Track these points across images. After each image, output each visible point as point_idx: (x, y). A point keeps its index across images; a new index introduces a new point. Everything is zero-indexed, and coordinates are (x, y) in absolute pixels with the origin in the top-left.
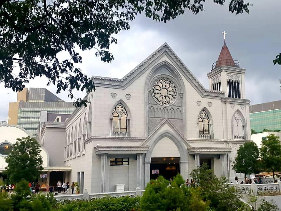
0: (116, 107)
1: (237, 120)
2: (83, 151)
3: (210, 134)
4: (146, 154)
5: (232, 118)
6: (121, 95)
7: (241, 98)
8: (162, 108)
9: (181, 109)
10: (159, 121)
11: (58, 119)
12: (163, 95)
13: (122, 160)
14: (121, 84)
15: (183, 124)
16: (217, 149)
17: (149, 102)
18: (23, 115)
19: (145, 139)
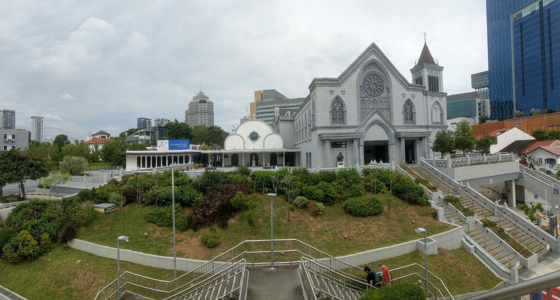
2: (309, 137)
3: (413, 121)
4: (360, 138)
5: (432, 108)
6: (337, 91)
7: (440, 92)
8: (372, 100)
9: (388, 101)
11: (288, 113)
13: (341, 143)
14: (337, 83)
15: (390, 113)
16: (419, 132)
18: (259, 111)
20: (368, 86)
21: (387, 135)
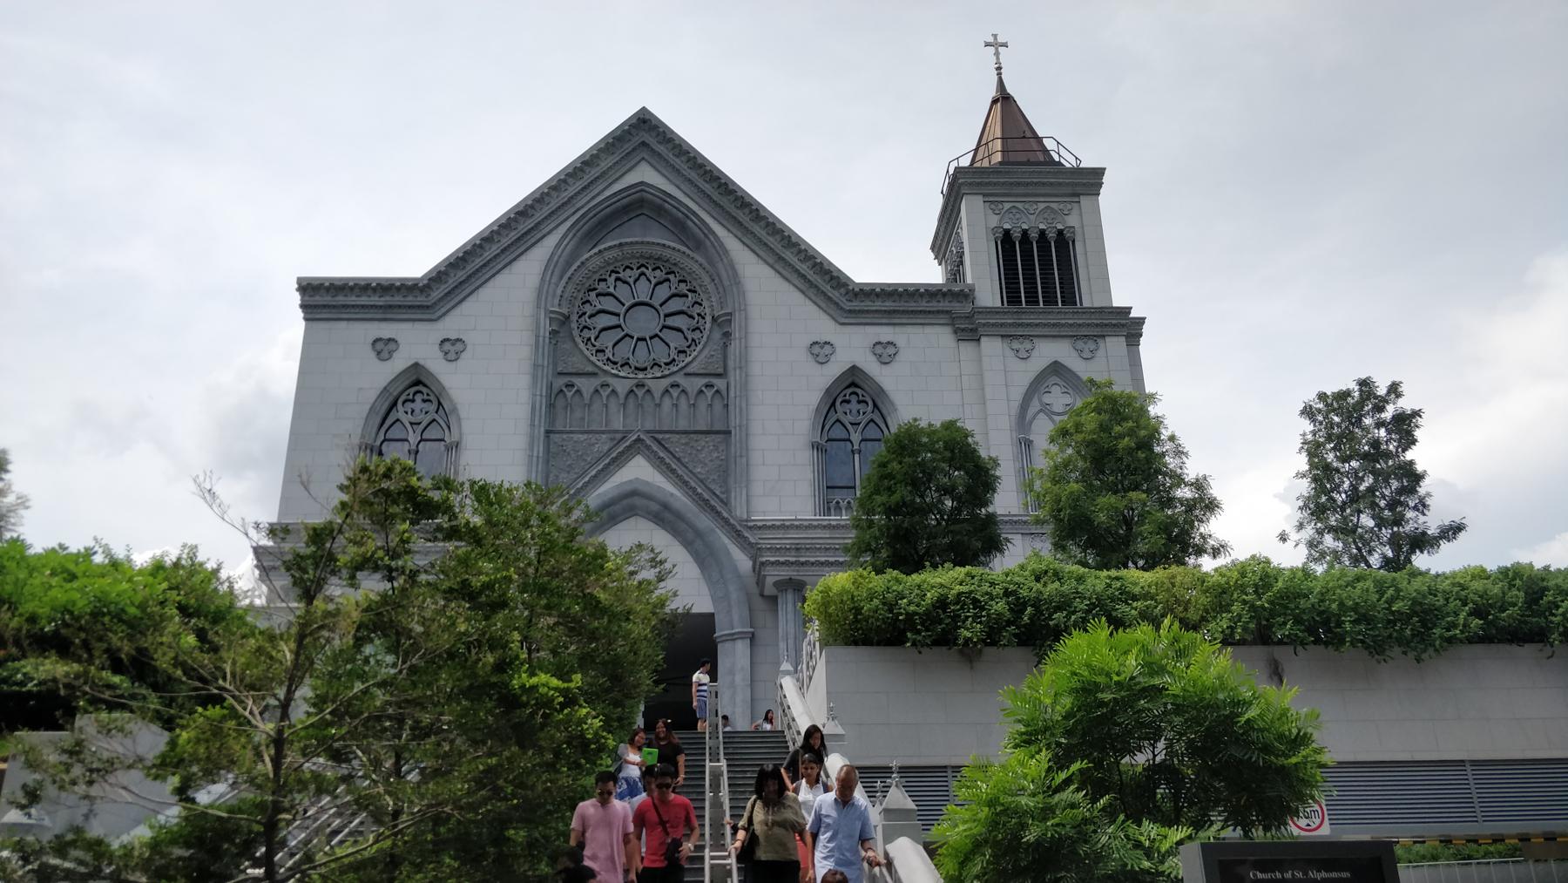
1: (1056, 418)
7: (1086, 304)
10: (606, 448)
12: (652, 334)
14: (421, 300)
17: (555, 365)
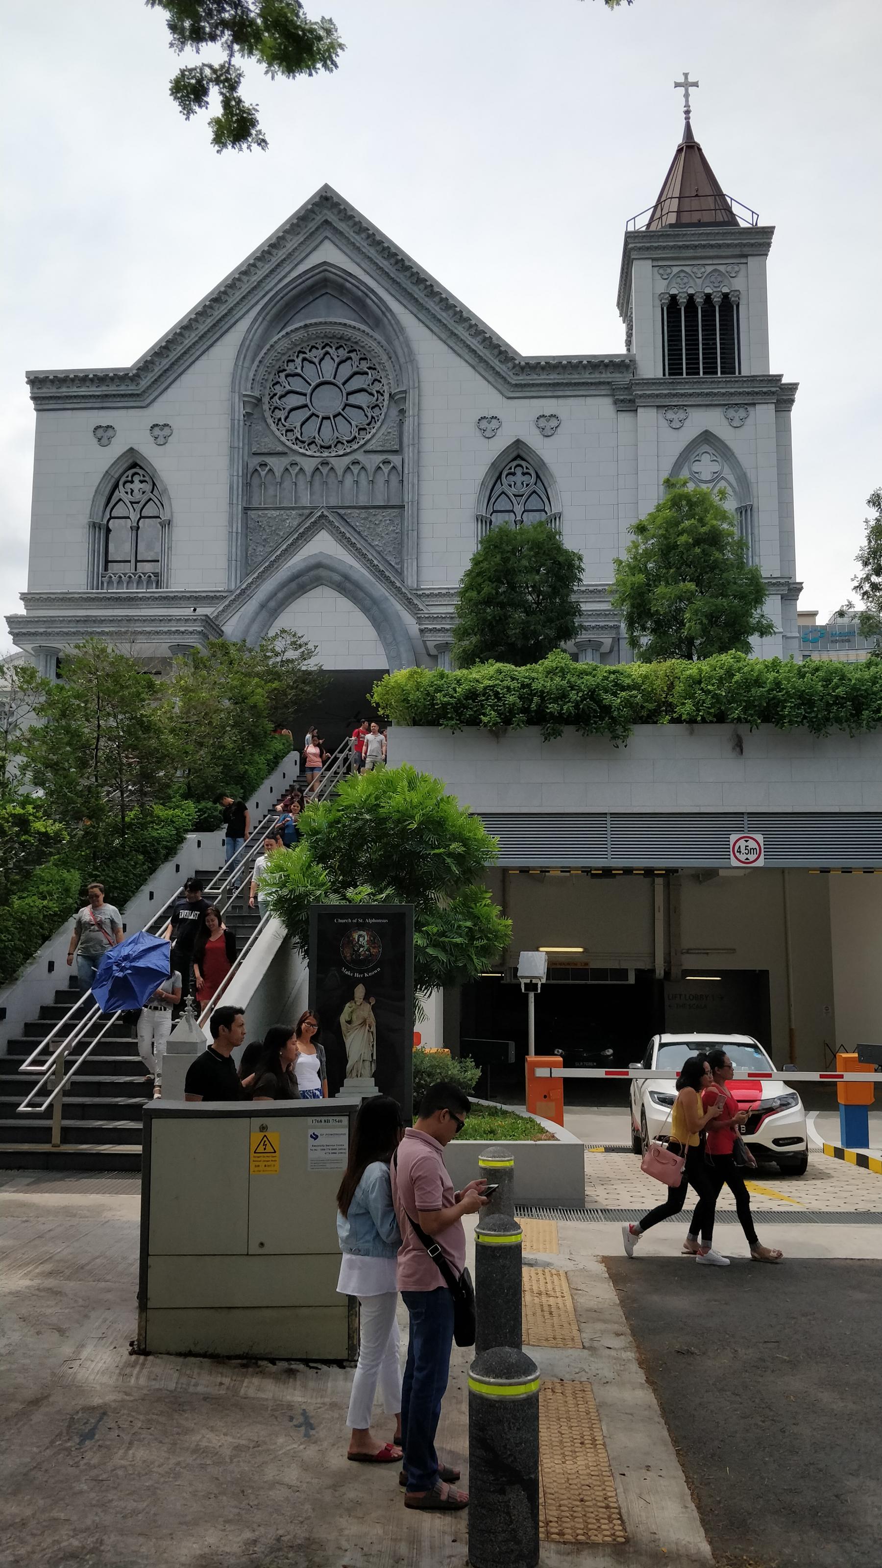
0: (504, 476)
12: (336, 412)
14: (131, 388)
19: (224, 594)
20: (314, 423)
21: (379, 644)
